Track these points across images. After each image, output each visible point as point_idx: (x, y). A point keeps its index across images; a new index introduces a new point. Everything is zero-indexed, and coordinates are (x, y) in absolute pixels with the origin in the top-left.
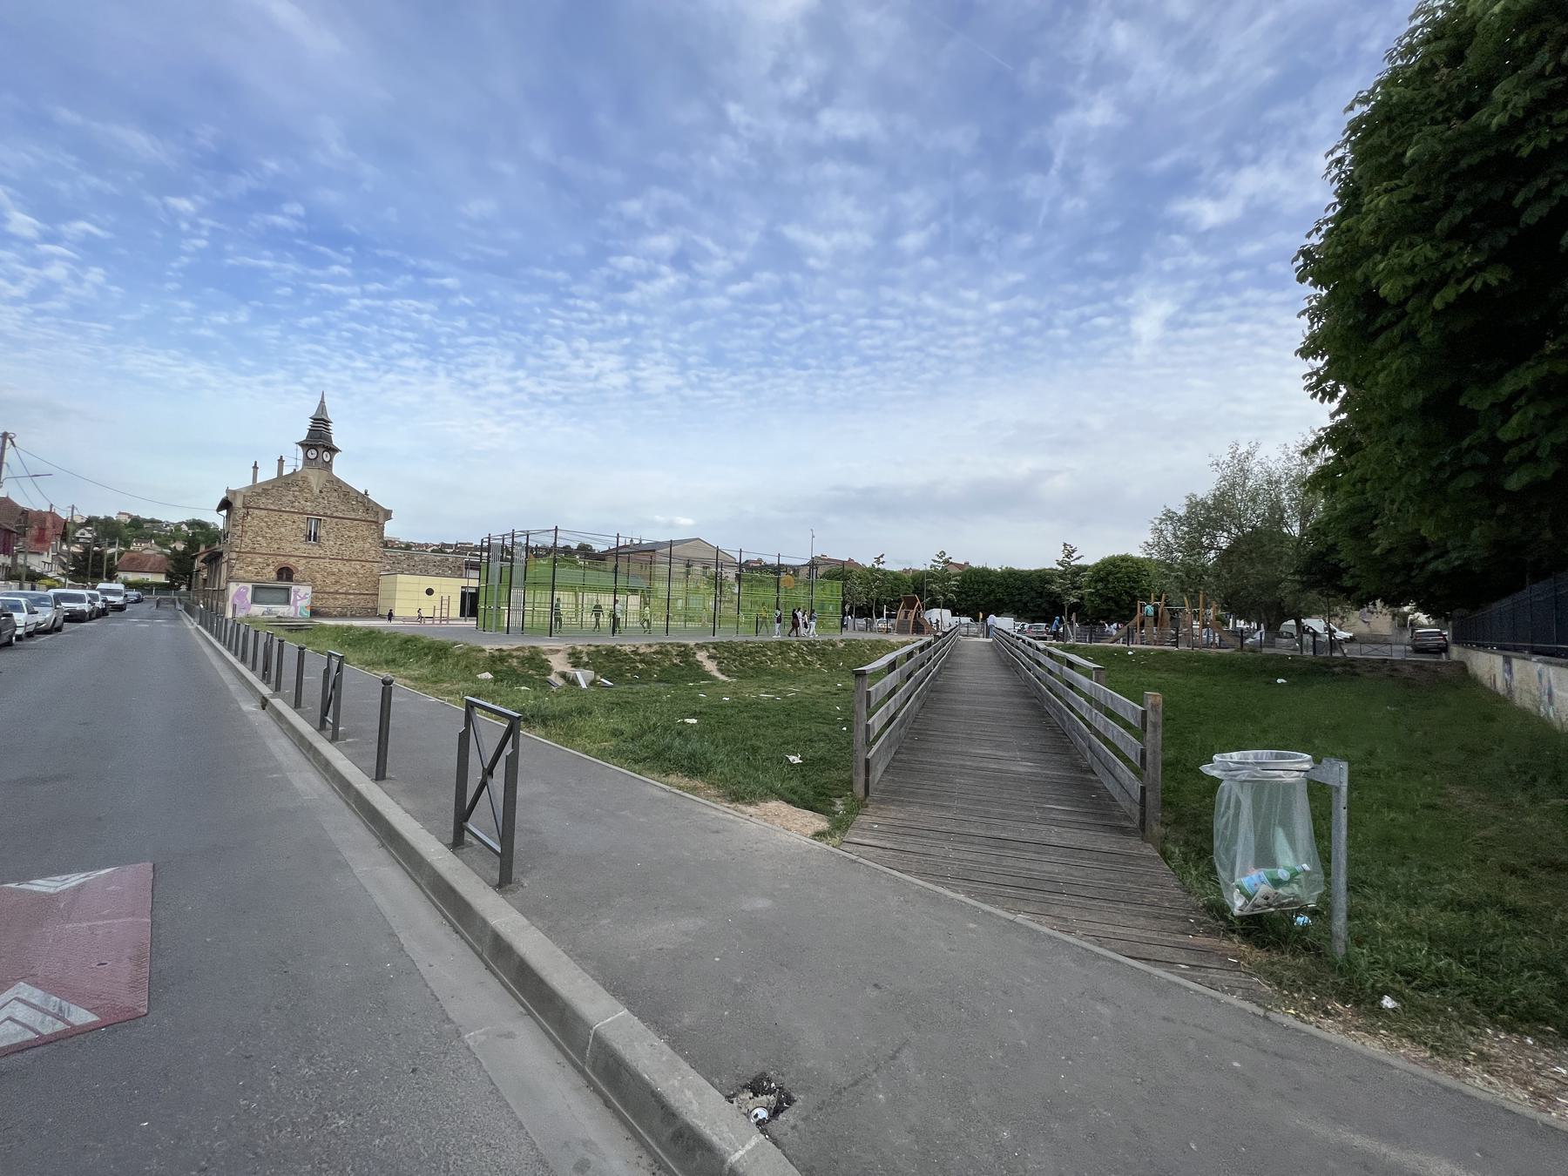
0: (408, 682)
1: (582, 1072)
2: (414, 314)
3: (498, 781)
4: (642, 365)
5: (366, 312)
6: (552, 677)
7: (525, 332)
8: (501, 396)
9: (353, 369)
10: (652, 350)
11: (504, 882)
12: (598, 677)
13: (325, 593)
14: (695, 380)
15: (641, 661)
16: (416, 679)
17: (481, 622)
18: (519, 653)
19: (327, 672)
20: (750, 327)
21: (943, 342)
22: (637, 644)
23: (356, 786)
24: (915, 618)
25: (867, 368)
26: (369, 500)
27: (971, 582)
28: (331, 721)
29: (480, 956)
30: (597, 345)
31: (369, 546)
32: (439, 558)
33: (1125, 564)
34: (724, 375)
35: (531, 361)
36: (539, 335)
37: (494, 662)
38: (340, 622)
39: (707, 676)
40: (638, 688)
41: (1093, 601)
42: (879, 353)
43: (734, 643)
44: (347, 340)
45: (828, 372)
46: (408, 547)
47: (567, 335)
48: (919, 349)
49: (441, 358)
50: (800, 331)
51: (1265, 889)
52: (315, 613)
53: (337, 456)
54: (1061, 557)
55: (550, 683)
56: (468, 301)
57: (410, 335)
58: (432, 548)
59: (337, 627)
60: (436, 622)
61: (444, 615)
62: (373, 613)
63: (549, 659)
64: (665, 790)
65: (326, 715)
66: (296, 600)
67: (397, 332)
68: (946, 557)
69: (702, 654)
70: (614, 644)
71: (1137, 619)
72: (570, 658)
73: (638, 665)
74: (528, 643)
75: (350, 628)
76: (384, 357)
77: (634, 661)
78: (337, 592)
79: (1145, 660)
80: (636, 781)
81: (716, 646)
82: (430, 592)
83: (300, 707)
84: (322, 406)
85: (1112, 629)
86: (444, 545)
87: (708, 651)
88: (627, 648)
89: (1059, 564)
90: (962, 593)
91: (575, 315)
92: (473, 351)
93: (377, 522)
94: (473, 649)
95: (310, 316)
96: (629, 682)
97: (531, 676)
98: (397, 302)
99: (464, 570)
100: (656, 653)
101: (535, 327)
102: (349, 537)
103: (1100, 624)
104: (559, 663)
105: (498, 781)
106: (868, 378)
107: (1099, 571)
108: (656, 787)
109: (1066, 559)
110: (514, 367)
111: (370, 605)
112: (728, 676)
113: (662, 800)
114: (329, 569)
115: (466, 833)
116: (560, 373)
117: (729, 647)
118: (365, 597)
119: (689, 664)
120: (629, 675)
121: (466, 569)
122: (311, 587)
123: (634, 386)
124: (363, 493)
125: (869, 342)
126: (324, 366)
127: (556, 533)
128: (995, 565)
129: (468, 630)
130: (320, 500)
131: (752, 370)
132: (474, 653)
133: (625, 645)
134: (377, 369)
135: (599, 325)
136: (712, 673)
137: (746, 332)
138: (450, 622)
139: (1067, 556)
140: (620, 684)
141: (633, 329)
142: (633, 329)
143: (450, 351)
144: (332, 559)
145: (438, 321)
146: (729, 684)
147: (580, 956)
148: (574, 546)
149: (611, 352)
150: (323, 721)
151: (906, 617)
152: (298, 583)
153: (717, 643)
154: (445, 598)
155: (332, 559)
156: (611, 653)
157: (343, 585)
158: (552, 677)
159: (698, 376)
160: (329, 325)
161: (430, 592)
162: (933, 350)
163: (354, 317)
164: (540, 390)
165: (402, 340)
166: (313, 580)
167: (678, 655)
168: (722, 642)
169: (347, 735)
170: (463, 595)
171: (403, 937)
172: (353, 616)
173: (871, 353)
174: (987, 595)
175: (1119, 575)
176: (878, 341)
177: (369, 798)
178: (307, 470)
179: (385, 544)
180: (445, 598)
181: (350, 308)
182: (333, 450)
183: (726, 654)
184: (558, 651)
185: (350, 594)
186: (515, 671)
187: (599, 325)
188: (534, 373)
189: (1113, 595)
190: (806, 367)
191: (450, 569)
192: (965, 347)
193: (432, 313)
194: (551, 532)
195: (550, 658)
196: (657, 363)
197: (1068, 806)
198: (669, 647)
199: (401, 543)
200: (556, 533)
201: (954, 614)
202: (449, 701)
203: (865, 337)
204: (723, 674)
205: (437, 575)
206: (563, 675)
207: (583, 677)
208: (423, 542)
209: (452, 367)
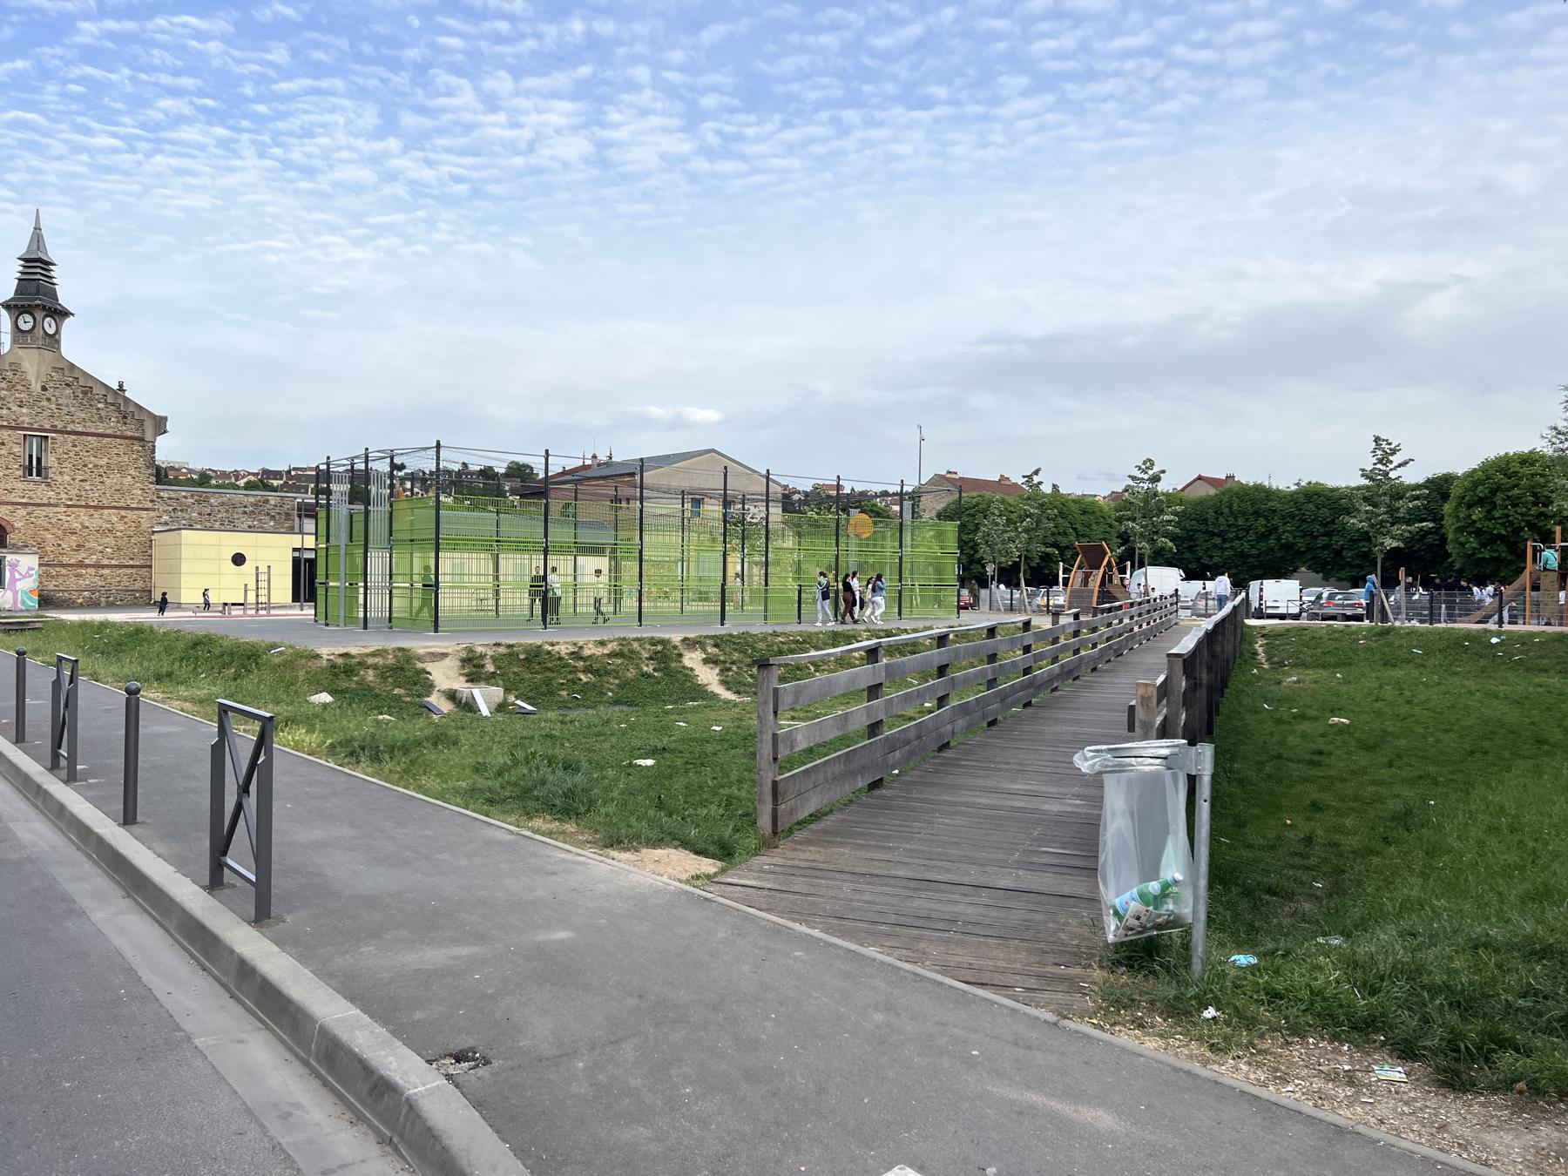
0: (188, 706)
1: (306, 1063)
2: (194, 43)
3: (251, 802)
4: (615, 117)
5: (110, 45)
6: (434, 699)
7: (394, 65)
8: (357, 189)
9: (92, 151)
10: (633, 86)
11: (262, 914)
12: (511, 698)
13: (63, 566)
14: (714, 140)
15: (586, 670)
16: (201, 702)
17: (321, 609)
18: (376, 660)
19: (57, 685)
20: (818, 30)
21: (1200, 35)
22: (581, 641)
23: (97, 830)
24: (1103, 584)
25: (1050, 98)
26: (127, 400)
27: (1232, 513)
28: (66, 755)
29: (225, 986)
30: (530, 82)
31: (136, 485)
32: (252, 500)
33: (1526, 470)
34: (769, 127)
35: (409, 120)
36: (421, 70)
37: (336, 675)
38: (88, 616)
39: (700, 692)
40: (576, 713)
41: (1463, 544)
42: (1070, 65)
43: (752, 636)
44: (78, 98)
45: (974, 109)
46: (204, 478)
47: (472, 67)
48: (1152, 52)
49: (245, 124)
50: (915, 30)
51: (1135, 907)
52: (46, 601)
53: (68, 323)
54: (1369, 463)
55: (430, 709)
56: (289, 12)
57: (186, 82)
58: (246, 480)
59: (83, 624)
60: (250, 612)
61: (263, 599)
62: (143, 598)
63: (428, 669)
64: (511, 832)
65: (60, 748)
66: (14, 581)
67: (165, 79)
68: (1156, 469)
69: (693, 655)
70: (539, 642)
71: (1526, 578)
72: (463, 667)
73: (582, 677)
74: (393, 643)
75: (104, 625)
76: (143, 126)
77: (575, 670)
78: (81, 565)
79: (1522, 652)
80: (477, 824)
81: (718, 642)
82: (239, 559)
83: (23, 741)
84: (37, 238)
85: (1484, 594)
86: (267, 473)
87: (704, 650)
88: (563, 647)
89: (1367, 477)
90: (1214, 534)
91: (486, 26)
92: (301, 106)
93: (141, 439)
94: (300, 655)
95: (12, 60)
96: (564, 705)
97: (398, 698)
98: (161, 22)
99: (297, 519)
100: (613, 655)
101: (413, 54)
102: (95, 466)
103: (1463, 588)
104: (445, 676)
105: (251, 802)
106: (1051, 118)
107: (1476, 484)
108: (502, 828)
109: (1379, 466)
110: (379, 134)
111: (139, 585)
112: (738, 692)
113: (501, 843)
114: (66, 525)
115: (226, 870)
116: (462, 141)
117: (741, 643)
118: (129, 571)
119: (670, 674)
120: (564, 693)
121: (300, 516)
122: (37, 556)
123: (601, 157)
124: (116, 387)
125: (1051, 44)
126: (40, 150)
127: (438, 452)
128: (1285, 481)
129: (300, 625)
130: (45, 403)
131: (824, 115)
132: (304, 661)
133: (558, 643)
134: (133, 150)
135: (530, 43)
136: (710, 689)
137: (810, 40)
138: (273, 612)
139: (1380, 461)
140: (546, 709)
141: (597, 47)
142: (597, 47)
143: (261, 108)
144: (69, 506)
145: (237, 54)
146: (735, 705)
147: (325, 974)
148: (501, 469)
149: (555, 95)
150: (56, 756)
151: (1085, 582)
152: (17, 549)
153: (720, 638)
154: (263, 569)
155: (69, 506)
156: (535, 656)
157: (92, 551)
158: (434, 699)
159: (719, 133)
160: (45, 74)
161: (239, 559)
162: (1180, 51)
163: (89, 55)
164: (428, 174)
165: (175, 93)
166: (41, 545)
167: (651, 658)
168: (731, 635)
169: (88, 774)
170: (296, 562)
171: (147, 976)
172: (111, 606)
173: (1054, 65)
174: (1263, 537)
175: (1516, 491)
176: (1069, 42)
177: (113, 843)
178: (20, 351)
179: (162, 476)
180: (263, 569)
181: (79, 39)
182: (61, 314)
183: (736, 656)
184: (444, 655)
185: (103, 567)
186: (371, 689)
187: (530, 43)
188: (416, 141)
189: (1503, 532)
190: (927, 103)
191: (273, 517)
192: (1247, 42)
193: (225, 39)
194: (428, 452)
195: (429, 667)
196: (643, 112)
197: (1077, 850)
198: (636, 645)
199: (191, 471)
200: (438, 452)
201: (1189, 576)
202: (245, 731)
203: (1042, 36)
204: (728, 689)
205: (251, 529)
206: (452, 696)
207: (485, 698)
208: (229, 469)
209: (266, 139)
